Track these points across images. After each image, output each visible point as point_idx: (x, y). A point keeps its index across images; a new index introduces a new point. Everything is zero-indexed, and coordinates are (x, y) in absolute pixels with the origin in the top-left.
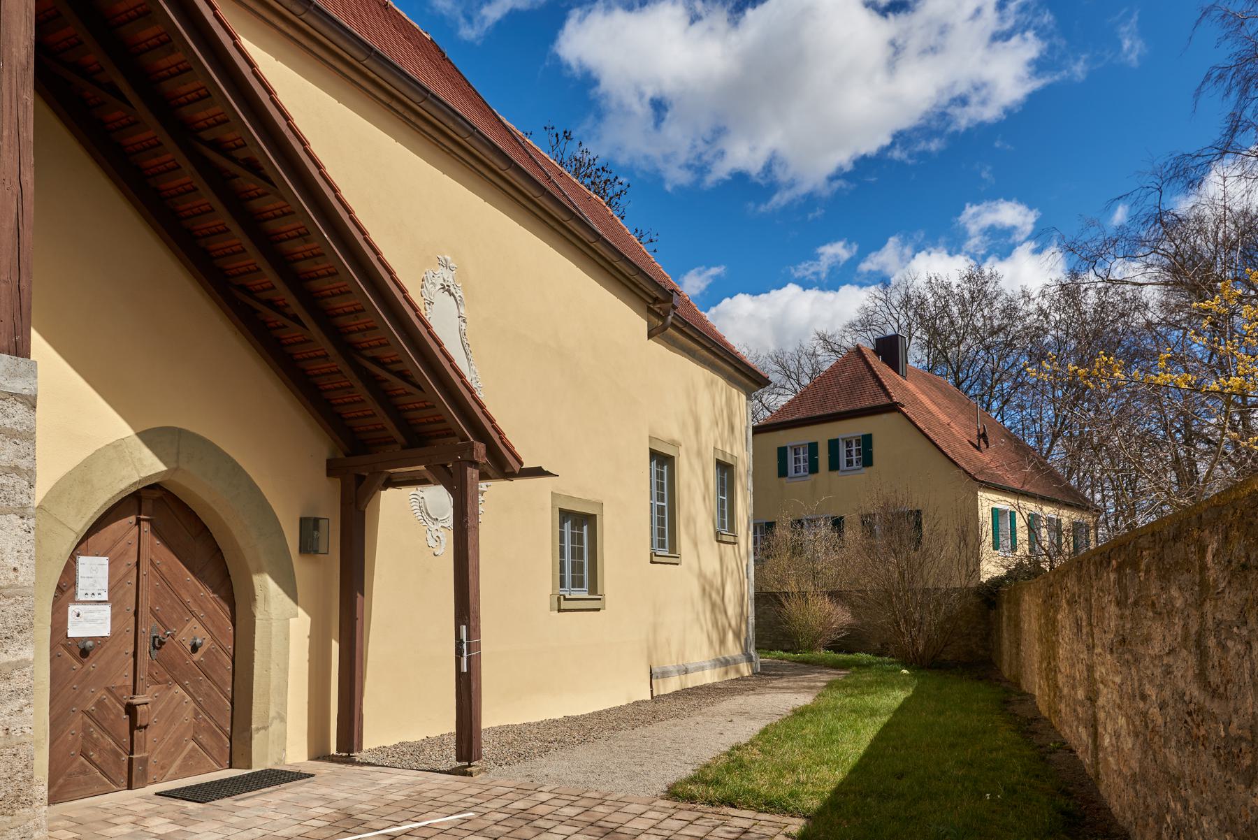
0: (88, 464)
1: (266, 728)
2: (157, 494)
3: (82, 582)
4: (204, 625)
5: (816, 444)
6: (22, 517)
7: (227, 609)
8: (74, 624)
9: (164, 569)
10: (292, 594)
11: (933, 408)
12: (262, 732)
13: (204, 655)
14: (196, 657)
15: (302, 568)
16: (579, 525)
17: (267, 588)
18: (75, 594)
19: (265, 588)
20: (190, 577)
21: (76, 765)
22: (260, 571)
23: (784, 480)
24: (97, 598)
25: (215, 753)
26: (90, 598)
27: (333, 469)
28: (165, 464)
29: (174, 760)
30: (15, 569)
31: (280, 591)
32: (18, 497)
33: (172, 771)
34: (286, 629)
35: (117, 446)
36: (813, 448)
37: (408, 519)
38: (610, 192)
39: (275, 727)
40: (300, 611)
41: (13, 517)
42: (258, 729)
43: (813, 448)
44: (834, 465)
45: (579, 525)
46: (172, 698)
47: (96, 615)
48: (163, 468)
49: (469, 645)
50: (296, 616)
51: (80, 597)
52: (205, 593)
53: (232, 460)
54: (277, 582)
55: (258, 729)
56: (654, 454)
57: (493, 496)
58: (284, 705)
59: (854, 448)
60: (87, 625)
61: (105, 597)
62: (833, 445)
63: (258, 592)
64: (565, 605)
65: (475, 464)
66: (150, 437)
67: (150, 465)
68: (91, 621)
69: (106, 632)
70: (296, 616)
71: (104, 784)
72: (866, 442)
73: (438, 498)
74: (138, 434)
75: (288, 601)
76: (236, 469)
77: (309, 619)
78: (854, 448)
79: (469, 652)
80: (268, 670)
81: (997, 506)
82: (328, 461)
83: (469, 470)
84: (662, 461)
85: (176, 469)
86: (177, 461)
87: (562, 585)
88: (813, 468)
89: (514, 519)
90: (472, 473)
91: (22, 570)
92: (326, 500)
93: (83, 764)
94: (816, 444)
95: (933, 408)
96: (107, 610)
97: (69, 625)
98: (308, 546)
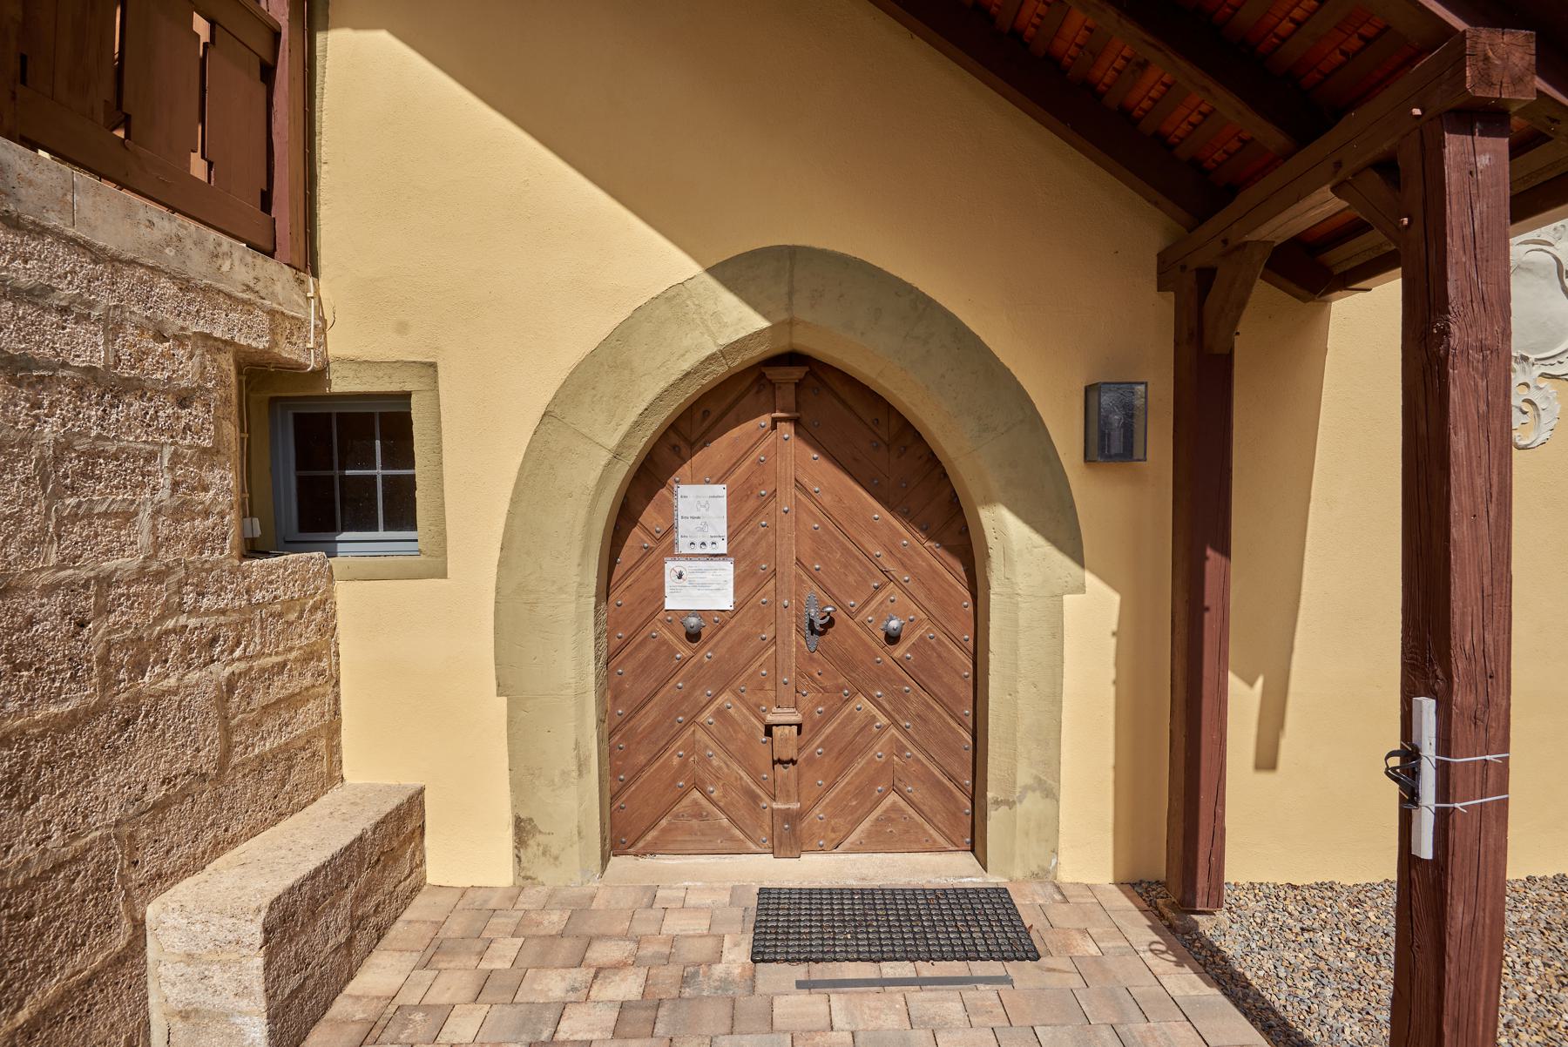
0: (621, 335)
1: (1010, 804)
2: (797, 373)
3: (684, 527)
4: (911, 596)
7: (960, 569)
8: (673, 591)
9: (827, 500)
10: (1072, 547)
12: (1004, 808)
13: (914, 648)
14: (900, 651)
15: (1094, 496)
17: (1006, 530)
18: (674, 544)
19: (1002, 533)
20: (879, 511)
21: (686, 802)
22: (989, 501)
24: (709, 550)
25: (938, 819)
26: (698, 551)
27: (1168, 271)
28: (766, 316)
29: (859, 821)
31: (1037, 539)
33: (853, 837)
34: (1063, 622)
35: (672, 297)
39: (1031, 804)
40: (1090, 579)
42: (997, 803)
46: (851, 717)
47: (709, 576)
48: (760, 323)
49: (1443, 770)
50: (1081, 589)
51: (683, 547)
52: (908, 537)
53: (911, 289)
54: (1027, 521)
55: (997, 803)
58: (1053, 764)
60: (695, 592)
61: (722, 547)
63: (991, 541)
65: (1484, 117)
66: (734, 273)
67: (737, 321)
68: (701, 585)
69: (726, 602)
70: (1081, 589)
71: (732, 838)
74: (709, 271)
75: (1061, 562)
76: (924, 307)
77: (1116, 598)
79: (1443, 792)
80: (1013, 693)
82: (1161, 257)
83: (1454, 145)
85: (791, 323)
86: (789, 307)
90: (1477, 163)
93: (696, 803)
96: (727, 569)
97: (667, 590)
98: (1110, 443)
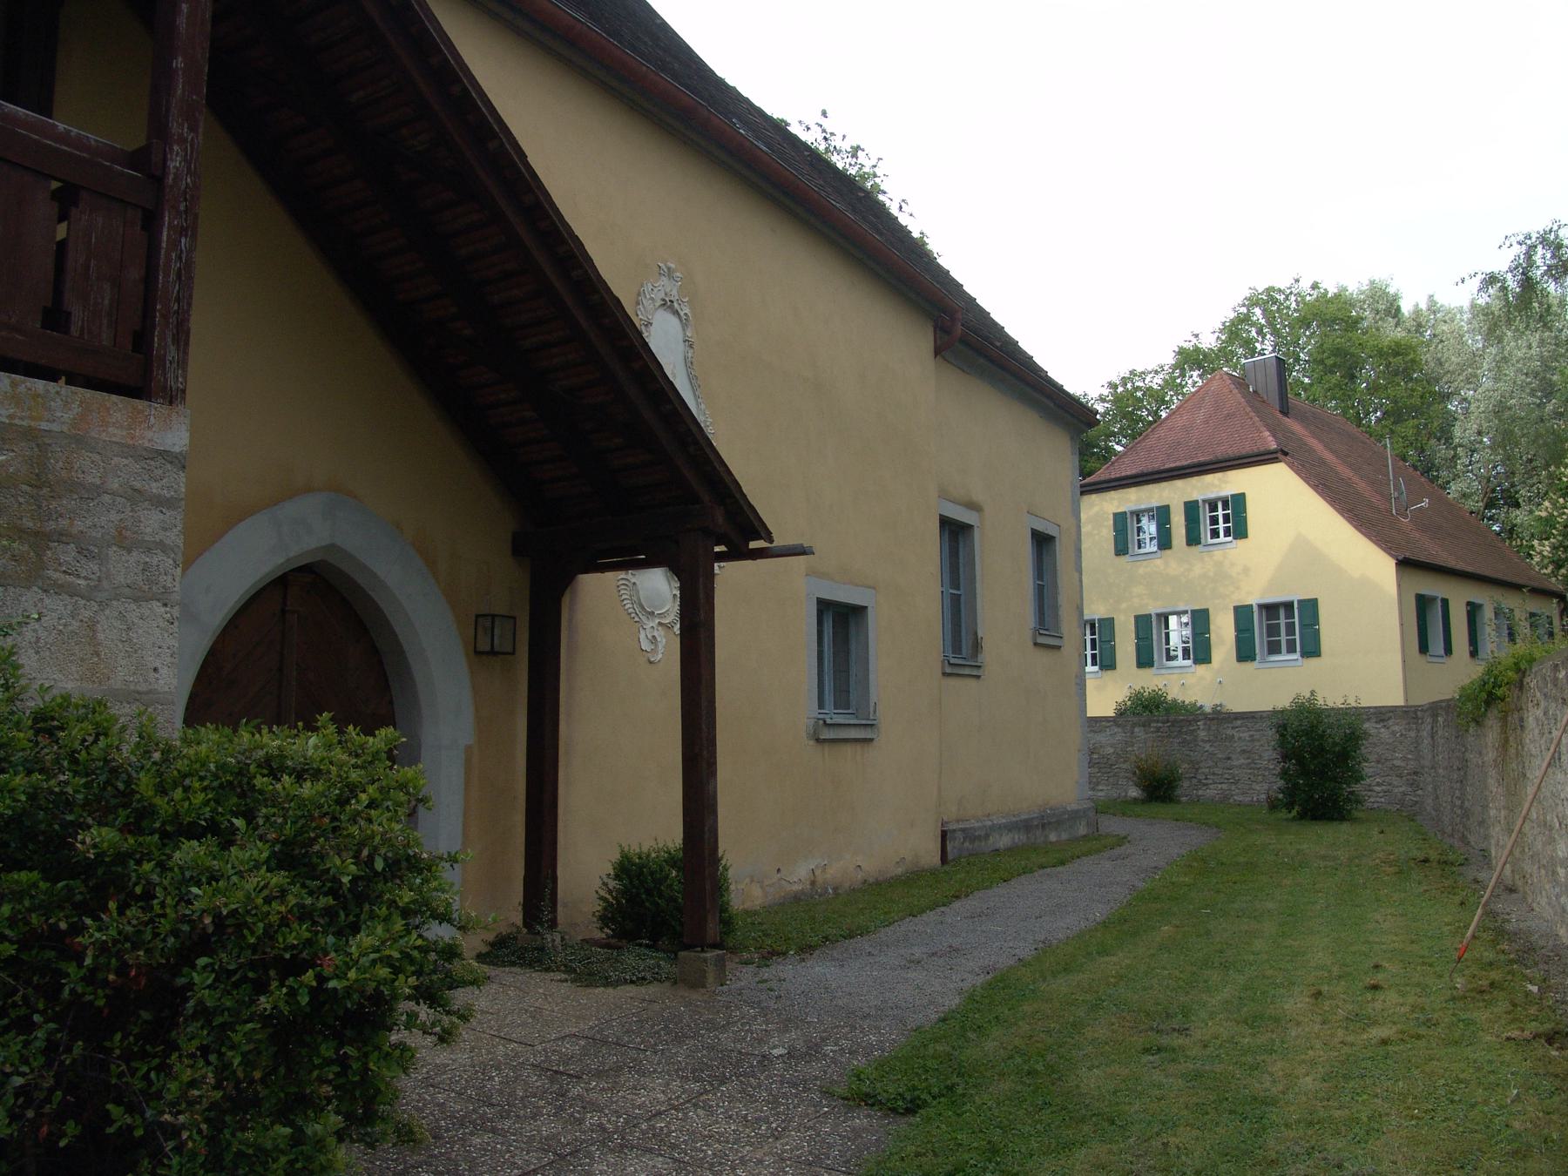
5: (1168, 507)
6: (165, 605)
11: (1328, 456)
16: (841, 622)
23: (1124, 559)
27: (520, 547)
30: (155, 670)
32: (162, 578)
36: (1191, 509)
37: (628, 613)
38: (1427, 763)
41: (155, 603)
43: (1162, 515)
44: (1193, 539)
45: (841, 622)
56: (945, 522)
57: (730, 577)
59: (1220, 513)
62: (1191, 509)
64: (827, 734)
72: (1237, 504)
73: (657, 587)
78: (1220, 513)
81: (1422, 592)
84: (955, 533)
87: (821, 705)
88: (1164, 542)
89: (760, 607)
91: (164, 671)
92: (507, 587)
94: (1168, 507)
95: (1328, 456)
